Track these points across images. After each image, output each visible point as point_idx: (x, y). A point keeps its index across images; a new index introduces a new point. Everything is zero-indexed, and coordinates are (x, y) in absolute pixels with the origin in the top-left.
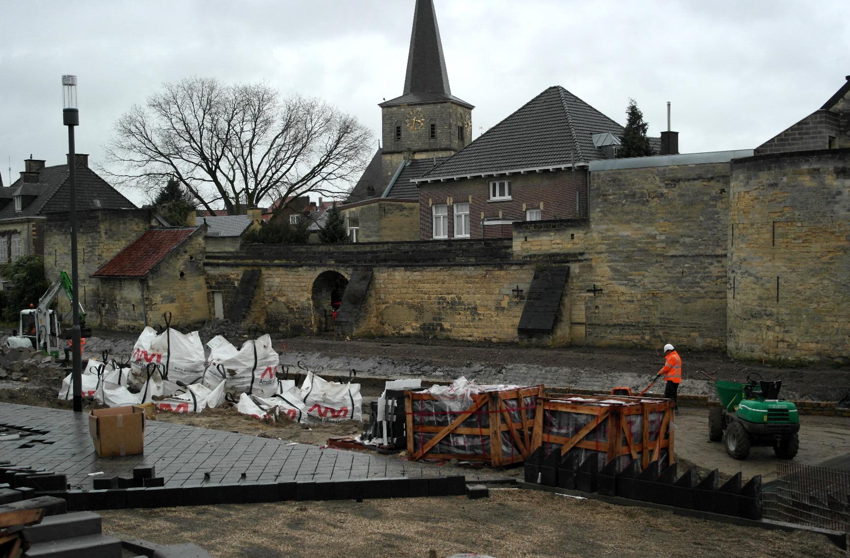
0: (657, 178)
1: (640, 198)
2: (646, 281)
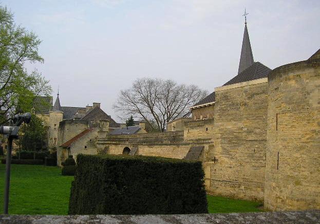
0: (244, 94)
1: (235, 105)
2: (237, 155)
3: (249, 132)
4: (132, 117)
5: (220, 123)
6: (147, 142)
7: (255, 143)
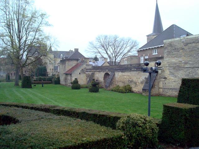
1: (176, 50)
3: (186, 63)
4: (96, 56)
5: (168, 59)
6: (120, 70)
7: (189, 69)
